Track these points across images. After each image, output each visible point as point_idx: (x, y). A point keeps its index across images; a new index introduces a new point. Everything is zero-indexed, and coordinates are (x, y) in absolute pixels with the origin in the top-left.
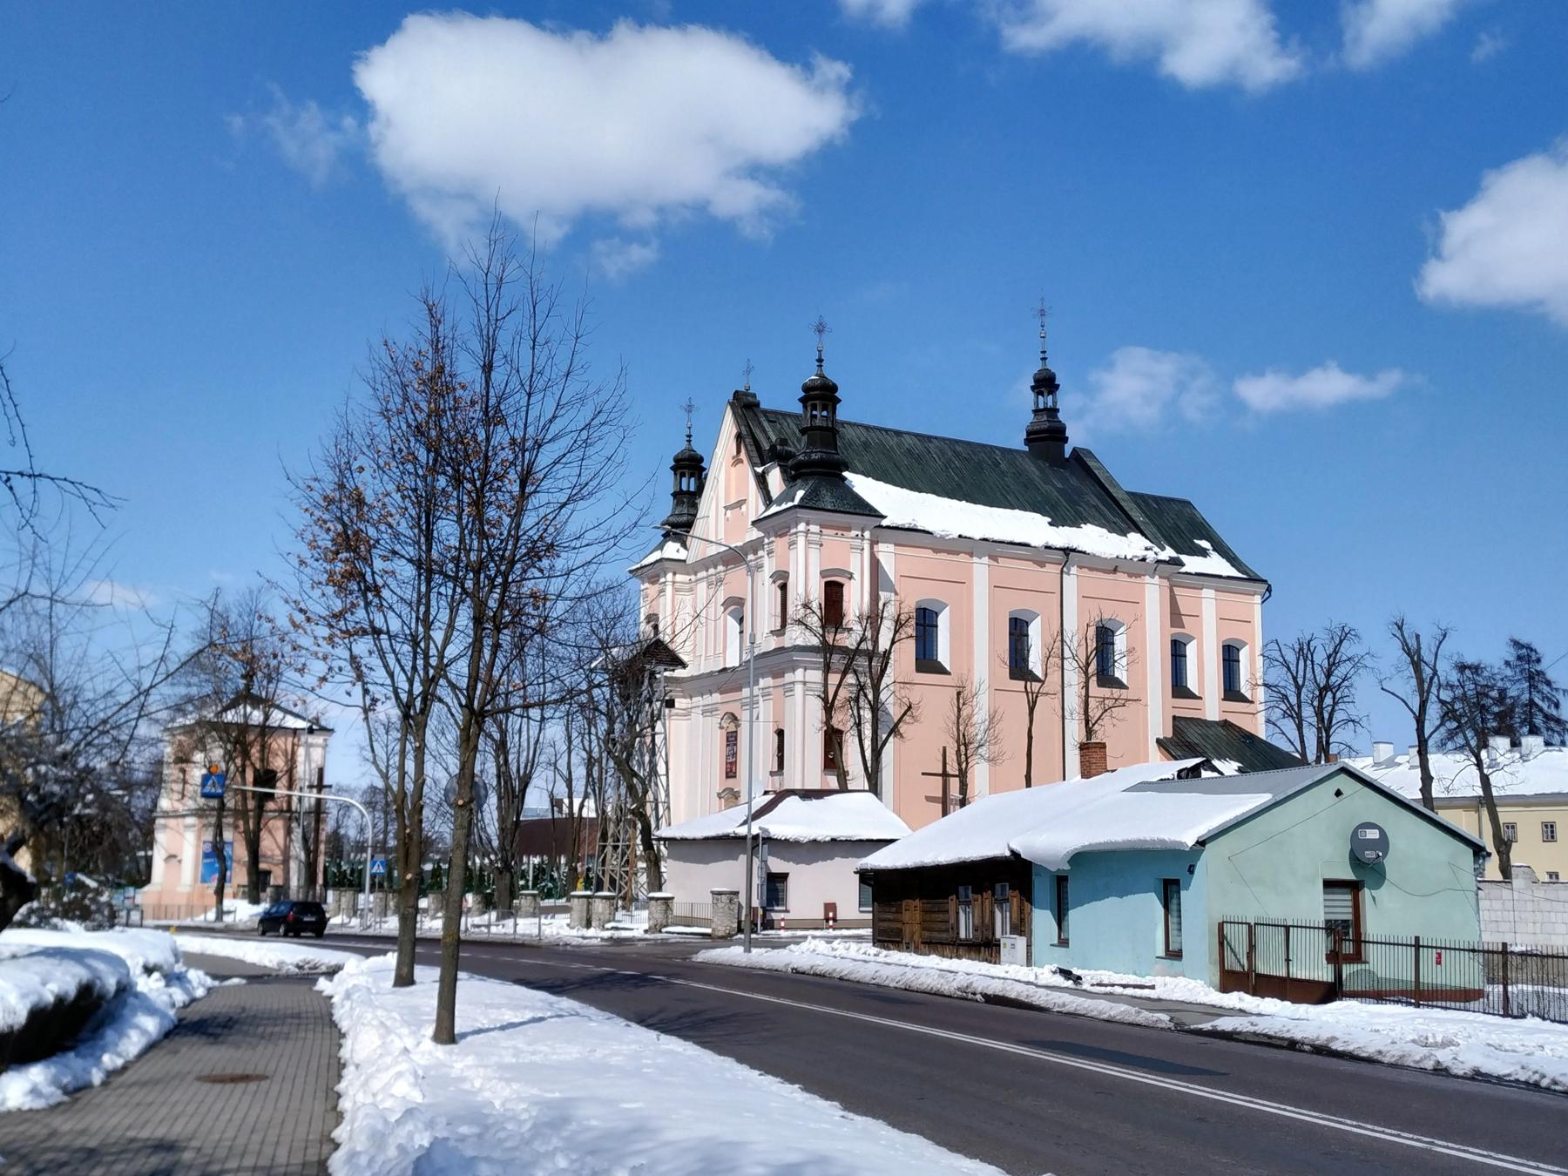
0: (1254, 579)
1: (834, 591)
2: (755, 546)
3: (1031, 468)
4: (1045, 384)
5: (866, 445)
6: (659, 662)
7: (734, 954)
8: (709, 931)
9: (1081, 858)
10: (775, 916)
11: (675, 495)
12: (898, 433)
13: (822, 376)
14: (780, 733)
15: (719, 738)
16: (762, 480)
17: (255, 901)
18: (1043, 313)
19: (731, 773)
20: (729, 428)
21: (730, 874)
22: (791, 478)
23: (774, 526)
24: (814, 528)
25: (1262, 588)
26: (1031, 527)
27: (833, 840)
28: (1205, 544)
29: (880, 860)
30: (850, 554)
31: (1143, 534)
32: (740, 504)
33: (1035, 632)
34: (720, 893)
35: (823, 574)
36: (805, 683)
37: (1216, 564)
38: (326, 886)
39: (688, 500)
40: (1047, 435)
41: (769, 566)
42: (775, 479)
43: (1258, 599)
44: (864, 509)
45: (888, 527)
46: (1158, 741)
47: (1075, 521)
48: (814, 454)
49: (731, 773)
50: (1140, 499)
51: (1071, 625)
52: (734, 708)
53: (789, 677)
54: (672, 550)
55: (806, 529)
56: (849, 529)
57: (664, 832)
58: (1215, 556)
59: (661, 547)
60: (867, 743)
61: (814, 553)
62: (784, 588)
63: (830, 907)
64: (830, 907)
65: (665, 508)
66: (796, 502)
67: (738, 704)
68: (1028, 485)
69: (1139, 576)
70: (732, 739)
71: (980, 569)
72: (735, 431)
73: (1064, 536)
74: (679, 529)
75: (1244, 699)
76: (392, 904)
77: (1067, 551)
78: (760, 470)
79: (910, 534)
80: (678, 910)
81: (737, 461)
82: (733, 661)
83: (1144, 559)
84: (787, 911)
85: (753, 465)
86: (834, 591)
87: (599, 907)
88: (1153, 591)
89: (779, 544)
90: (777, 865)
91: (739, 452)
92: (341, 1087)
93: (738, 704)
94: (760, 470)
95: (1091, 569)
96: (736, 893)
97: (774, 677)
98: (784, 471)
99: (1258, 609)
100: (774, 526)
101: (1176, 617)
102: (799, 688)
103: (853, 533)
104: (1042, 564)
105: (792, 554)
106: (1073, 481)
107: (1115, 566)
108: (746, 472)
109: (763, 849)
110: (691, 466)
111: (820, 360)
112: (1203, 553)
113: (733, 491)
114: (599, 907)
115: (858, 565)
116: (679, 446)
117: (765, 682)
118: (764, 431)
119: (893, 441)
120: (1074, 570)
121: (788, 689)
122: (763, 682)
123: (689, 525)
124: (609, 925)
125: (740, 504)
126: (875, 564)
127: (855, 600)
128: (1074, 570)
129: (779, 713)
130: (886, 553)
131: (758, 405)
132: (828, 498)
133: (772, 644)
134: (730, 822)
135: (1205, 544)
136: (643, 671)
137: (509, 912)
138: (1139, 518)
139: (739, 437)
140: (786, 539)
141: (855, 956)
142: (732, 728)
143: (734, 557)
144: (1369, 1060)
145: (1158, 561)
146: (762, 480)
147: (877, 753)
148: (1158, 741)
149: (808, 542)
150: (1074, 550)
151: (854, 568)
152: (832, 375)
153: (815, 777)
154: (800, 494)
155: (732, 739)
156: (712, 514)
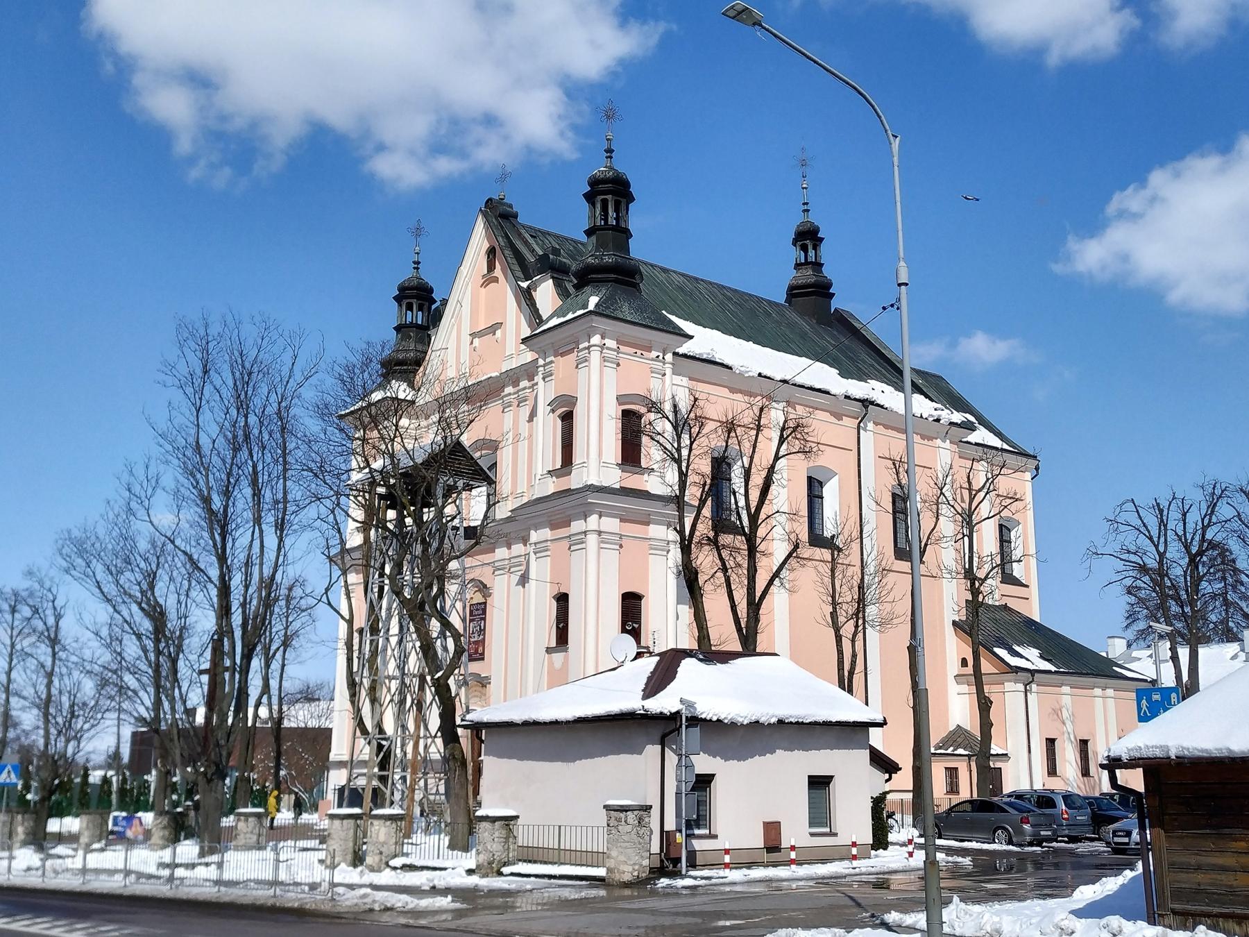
2: (528, 371)
4: (808, 237)
6: (459, 474)
8: (601, 872)
10: (698, 845)
11: (398, 329)
12: (665, 270)
13: (611, 168)
14: (562, 600)
16: (527, 298)
21: (638, 775)
24: (611, 343)
25: (1032, 464)
27: (780, 722)
31: (927, 396)
32: (493, 329)
34: (624, 809)
35: (621, 399)
36: (600, 533)
40: (812, 293)
41: (545, 392)
42: (546, 294)
43: (1028, 476)
45: (685, 356)
46: (954, 623)
47: (862, 376)
53: (577, 526)
54: (401, 390)
55: (600, 343)
56: (649, 350)
57: (481, 714)
60: (740, 595)
61: (610, 372)
62: (567, 418)
63: (772, 830)
64: (772, 830)
66: (591, 307)
67: (489, 569)
68: (803, 336)
69: (930, 439)
72: (486, 245)
73: (858, 389)
75: (1016, 582)
76: (20, 829)
77: (866, 403)
78: (525, 285)
80: (524, 836)
81: (489, 279)
83: (938, 420)
84: (713, 837)
85: (517, 279)
89: (562, 365)
90: (703, 763)
91: (491, 267)
93: (489, 569)
94: (525, 285)
95: (886, 427)
96: (648, 808)
97: (554, 526)
98: (558, 285)
99: (1029, 486)
102: (592, 539)
103: (654, 354)
104: (839, 416)
105: (582, 372)
109: (689, 736)
111: (609, 151)
116: (406, 274)
117: (543, 534)
118: (526, 243)
119: (662, 277)
120: (870, 426)
121: (577, 541)
122: (534, 536)
124: (397, 862)
125: (493, 329)
128: (870, 426)
129: (561, 570)
131: (516, 216)
132: (626, 308)
133: (551, 486)
134: (622, 692)
137: (215, 842)
139: (491, 252)
140: (572, 357)
142: (478, 598)
145: (952, 424)
146: (527, 298)
147: (755, 606)
148: (954, 623)
149: (604, 359)
150: (872, 403)
152: (623, 166)
154: (593, 301)
156: (452, 345)
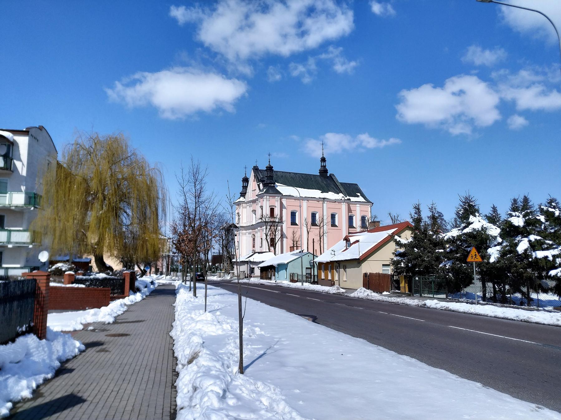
0: (368, 202)
1: (272, 210)
2: (257, 200)
3: (319, 179)
5: (282, 176)
7: (245, 281)
9: (279, 265)
12: (290, 173)
15: (252, 239)
16: (259, 186)
17: (157, 274)
18: (246, 168)
19: (254, 247)
20: (252, 174)
22: (265, 185)
23: (260, 196)
26: (316, 193)
28: (359, 194)
29: (262, 265)
30: (275, 202)
32: (255, 190)
33: (317, 216)
35: (270, 206)
37: (361, 199)
38: (171, 271)
39: (245, 188)
40: (324, 171)
42: (261, 185)
44: (278, 192)
48: (269, 179)
49: (254, 247)
50: (343, 184)
51: (325, 213)
52: (254, 233)
54: (242, 199)
58: (361, 197)
59: (239, 198)
61: (268, 202)
65: (241, 190)
70: (254, 240)
71: (305, 203)
73: (325, 195)
74: (243, 194)
77: (324, 198)
79: (289, 197)
82: (254, 223)
86: (272, 210)
87: (222, 274)
88: (344, 206)
92: (172, 334)
100: (260, 196)
101: (350, 210)
106: (329, 182)
107: (335, 201)
108: (256, 184)
110: (246, 180)
112: (358, 196)
113: (253, 186)
114: (222, 274)
115: (277, 205)
118: (116, 356)
119: (288, 175)
123: (246, 193)
125: (255, 190)
126: (281, 204)
127: (277, 212)
130: (284, 201)
135: (359, 194)
136: (230, 230)
138: (342, 189)
141: (363, 293)
143: (254, 201)
144: (453, 311)
146: (259, 186)
151: (277, 205)
153: (265, 247)
155: (254, 240)
